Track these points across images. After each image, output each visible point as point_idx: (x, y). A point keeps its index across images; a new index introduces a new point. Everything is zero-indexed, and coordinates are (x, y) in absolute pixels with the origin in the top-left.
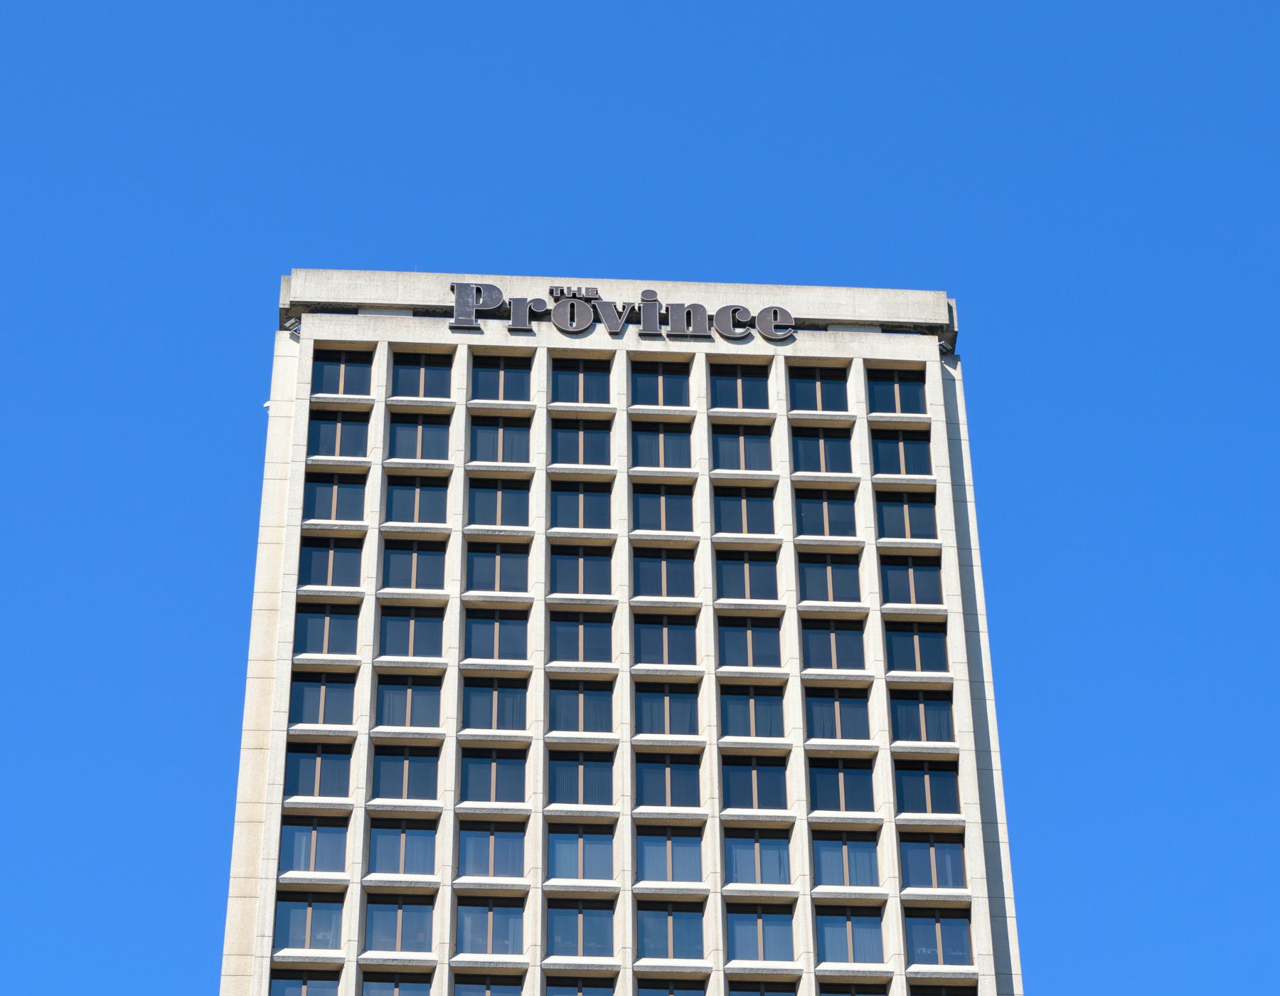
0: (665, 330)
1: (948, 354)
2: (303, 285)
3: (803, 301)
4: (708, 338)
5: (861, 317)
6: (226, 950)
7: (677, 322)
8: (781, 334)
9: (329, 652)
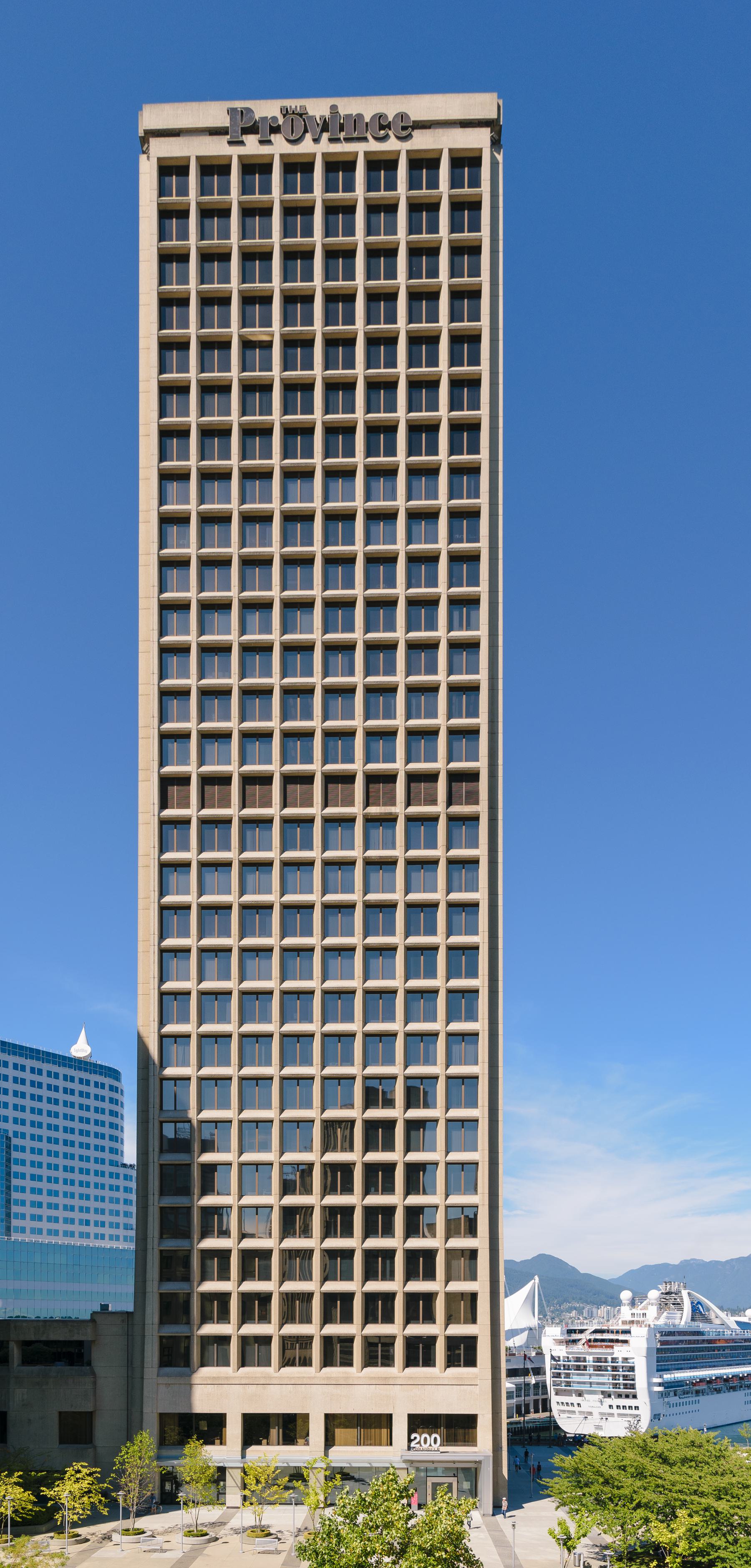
0: (342, 135)
1: (496, 143)
2: (153, 117)
3: (420, 106)
4: (365, 139)
5: (450, 115)
6: (140, 552)
7: (349, 126)
8: (405, 133)
9: (468, 454)
